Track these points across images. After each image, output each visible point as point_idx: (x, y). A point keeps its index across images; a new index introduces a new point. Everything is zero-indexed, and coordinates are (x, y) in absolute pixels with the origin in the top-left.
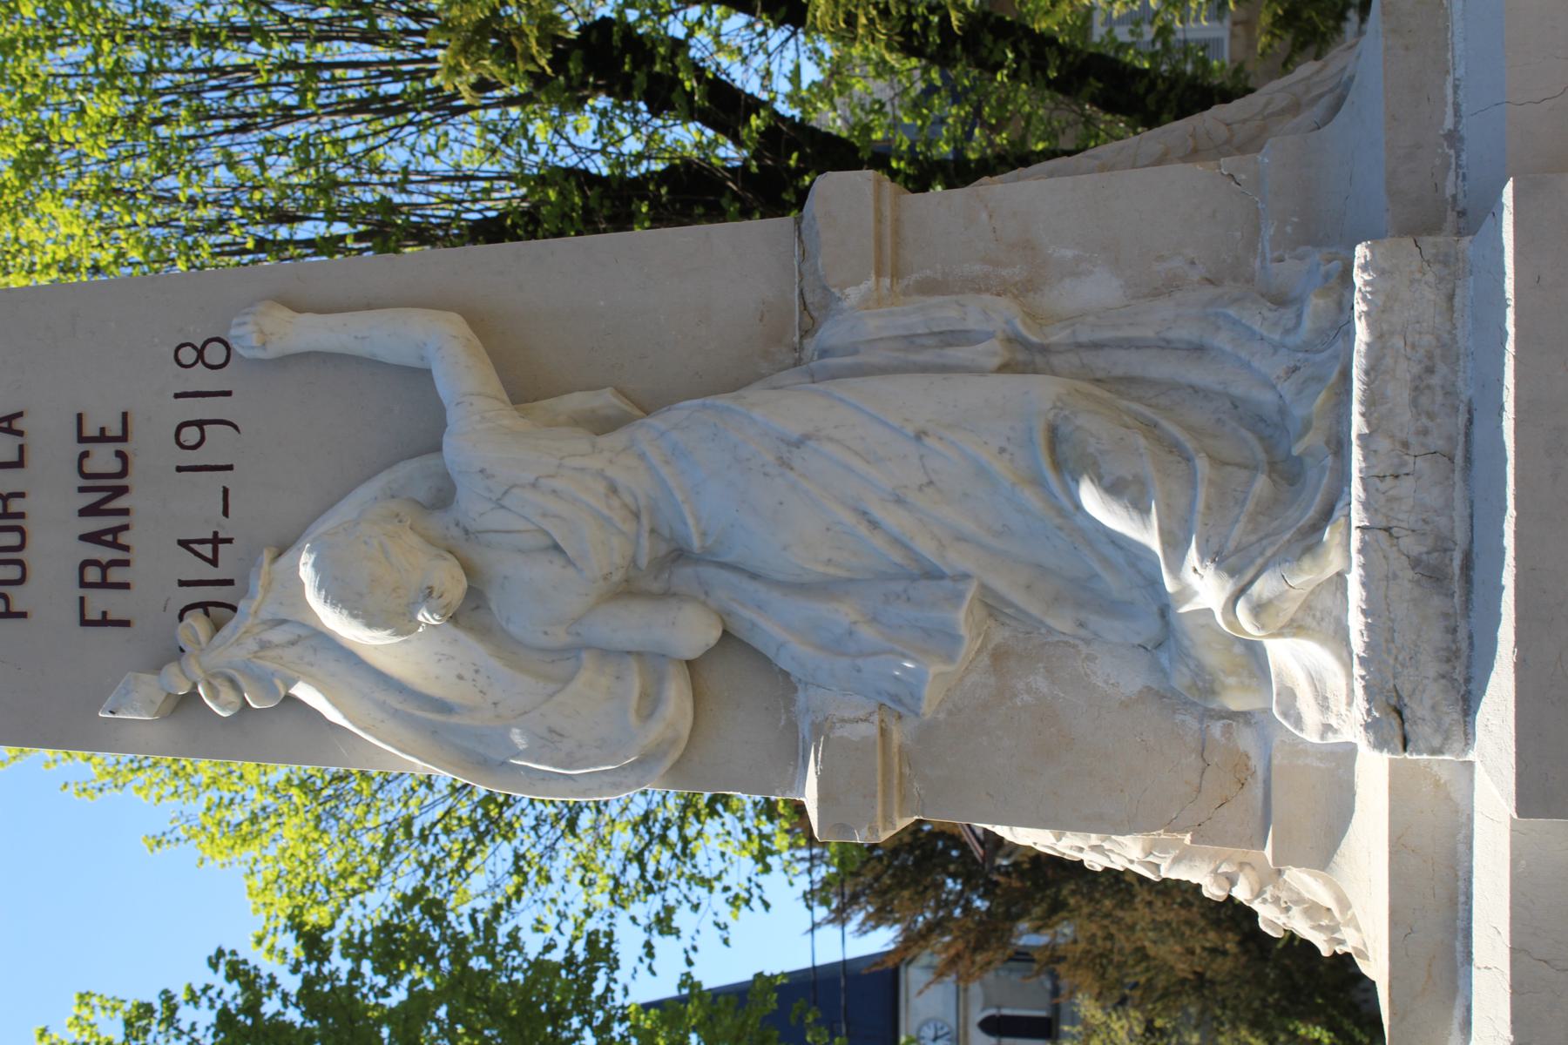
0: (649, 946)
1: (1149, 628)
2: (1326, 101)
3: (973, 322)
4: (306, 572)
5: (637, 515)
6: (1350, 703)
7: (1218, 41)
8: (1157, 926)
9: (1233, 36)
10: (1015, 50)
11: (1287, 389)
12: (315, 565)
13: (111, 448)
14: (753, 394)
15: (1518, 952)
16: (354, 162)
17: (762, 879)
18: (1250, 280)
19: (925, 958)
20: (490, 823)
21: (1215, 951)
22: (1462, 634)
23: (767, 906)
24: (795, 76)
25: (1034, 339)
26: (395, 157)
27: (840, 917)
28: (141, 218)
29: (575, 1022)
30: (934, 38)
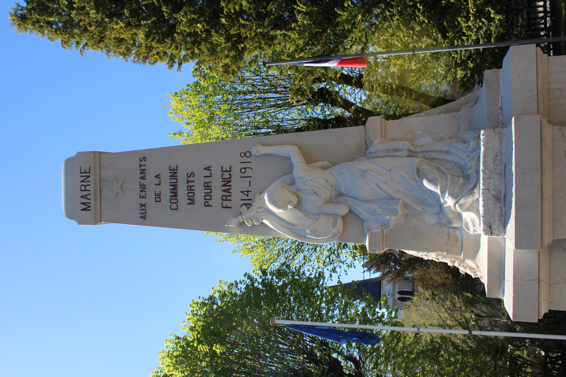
0: (331, 275)
1: (437, 210)
2: (474, 101)
3: (401, 147)
4: (266, 198)
5: (332, 186)
6: (480, 225)
7: (448, 90)
8: (435, 273)
9: (451, 89)
10: (406, 92)
11: (466, 160)
12: (268, 196)
13: (228, 173)
14: (355, 162)
15: (515, 277)
16: (271, 117)
17: (354, 262)
18: (458, 138)
19: (386, 279)
20: (299, 250)
21: (446, 278)
22: (504, 211)
23: (355, 267)
24: (361, 99)
25: (414, 150)
26: (281, 116)
27: (369, 270)
28: (231, 129)
29: (316, 289)
30: (389, 90)
